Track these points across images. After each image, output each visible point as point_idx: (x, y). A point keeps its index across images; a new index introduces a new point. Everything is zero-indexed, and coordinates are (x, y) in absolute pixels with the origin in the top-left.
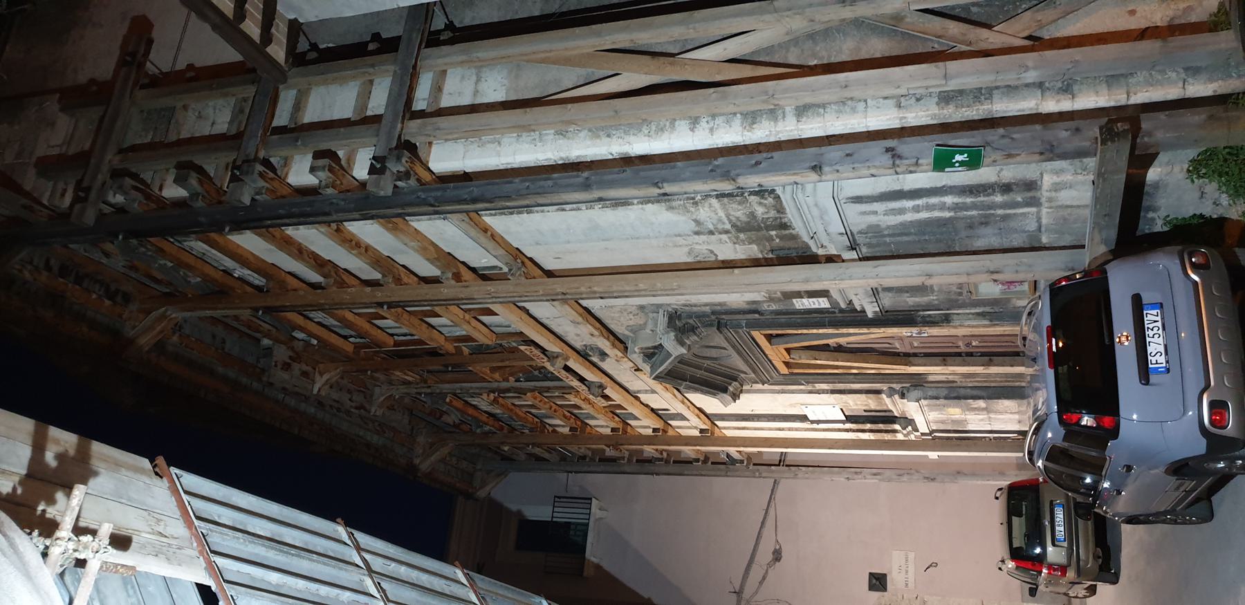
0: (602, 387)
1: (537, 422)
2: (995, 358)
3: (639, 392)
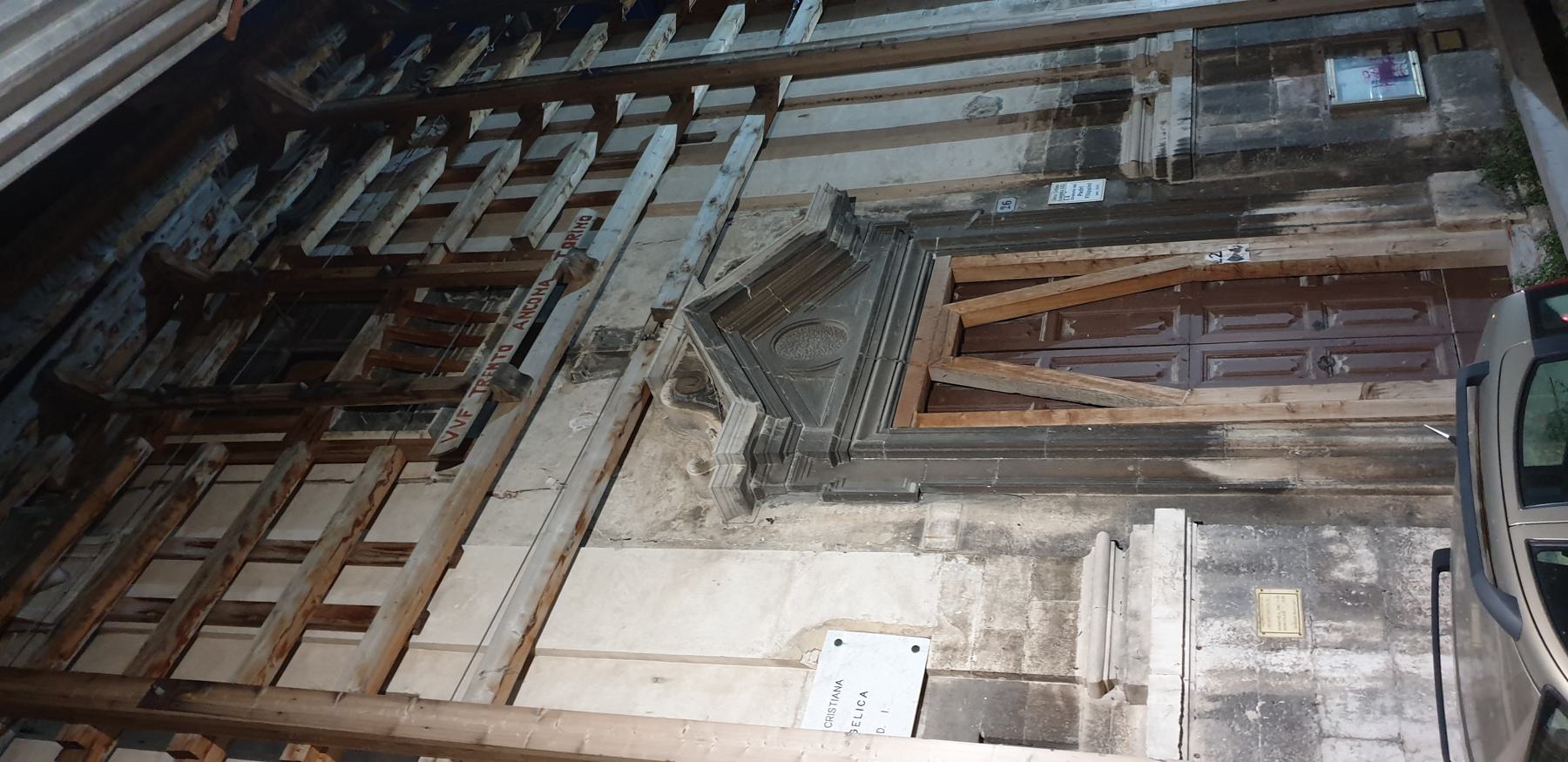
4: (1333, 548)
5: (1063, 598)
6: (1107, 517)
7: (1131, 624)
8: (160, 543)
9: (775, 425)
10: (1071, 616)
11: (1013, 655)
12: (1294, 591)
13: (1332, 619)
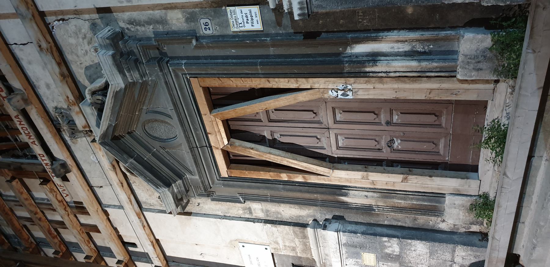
0: (64, 165)
1: (32, 242)
2: (413, 169)
3: (109, 206)
4: (386, 244)
5: (304, 239)
6: (311, 211)
7: (327, 257)
8: (7, 206)
9: (178, 184)
10: (308, 244)
11: (294, 252)
12: (373, 254)
13: (385, 262)
